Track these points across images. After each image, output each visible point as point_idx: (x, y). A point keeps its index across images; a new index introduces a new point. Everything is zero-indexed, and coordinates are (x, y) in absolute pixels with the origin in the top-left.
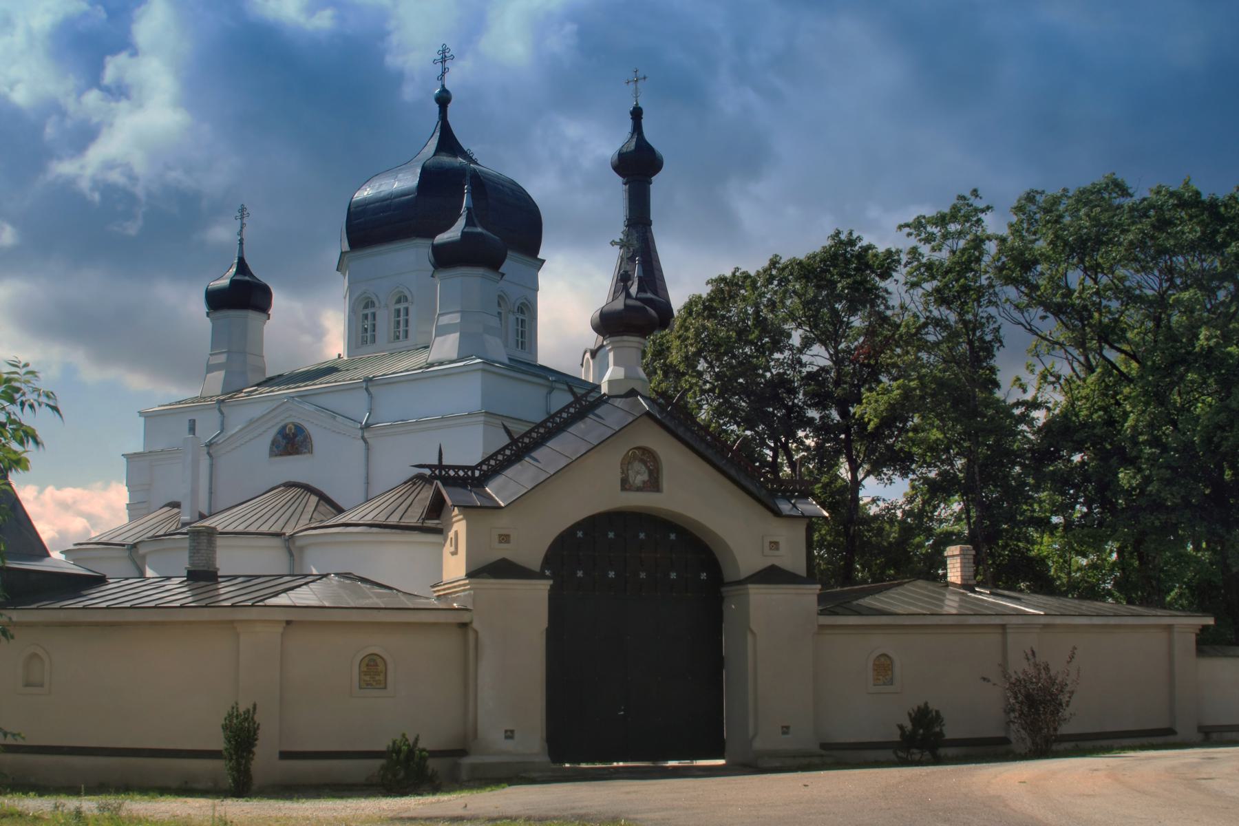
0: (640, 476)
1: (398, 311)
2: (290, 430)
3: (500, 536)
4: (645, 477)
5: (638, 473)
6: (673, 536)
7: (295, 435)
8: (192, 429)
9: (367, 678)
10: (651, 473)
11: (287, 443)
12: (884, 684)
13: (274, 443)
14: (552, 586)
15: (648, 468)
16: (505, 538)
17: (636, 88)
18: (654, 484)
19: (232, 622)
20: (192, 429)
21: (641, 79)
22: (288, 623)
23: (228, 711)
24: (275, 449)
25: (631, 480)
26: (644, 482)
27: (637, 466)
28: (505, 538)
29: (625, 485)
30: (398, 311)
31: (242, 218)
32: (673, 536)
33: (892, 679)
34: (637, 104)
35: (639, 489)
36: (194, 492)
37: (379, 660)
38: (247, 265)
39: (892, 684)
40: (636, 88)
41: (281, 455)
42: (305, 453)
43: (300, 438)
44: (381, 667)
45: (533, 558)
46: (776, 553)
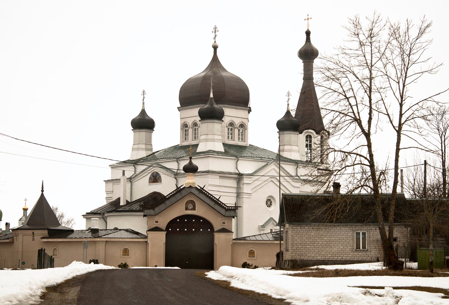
0: (190, 206)
1: (195, 129)
2: (155, 175)
3: (156, 221)
4: (192, 207)
5: (190, 206)
6: (201, 221)
7: (156, 176)
8: (124, 174)
9: (125, 253)
10: (193, 206)
11: (154, 178)
12: (252, 257)
13: (150, 178)
14: (166, 233)
15: (193, 205)
16: (157, 222)
17: (308, 22)
18: (194, 209)
19: (95, 241)
20: (124, 174)
21: (310, 19)
22: (106, 241)
23: (289, 292)
24: (150, 180)
25: (189, 208)
26: (192, 208)
27: (190, 204)
28: (157, 222)
29: (187, 209)
30: (195, 129)
31: (144, 95)
32: (201, 221)
33: (254, 256)
34: (308, 30)
35: (190, 210)
36: (125, 195)
37: (127, 249)
38: (145, 112)
39: (254, 257)
40: (308, 22)
41: (152, 183)
42: (159, 182)
43: (158, 177)
44: (128, 251)
45: (164, 226)
46: (224, 225)
